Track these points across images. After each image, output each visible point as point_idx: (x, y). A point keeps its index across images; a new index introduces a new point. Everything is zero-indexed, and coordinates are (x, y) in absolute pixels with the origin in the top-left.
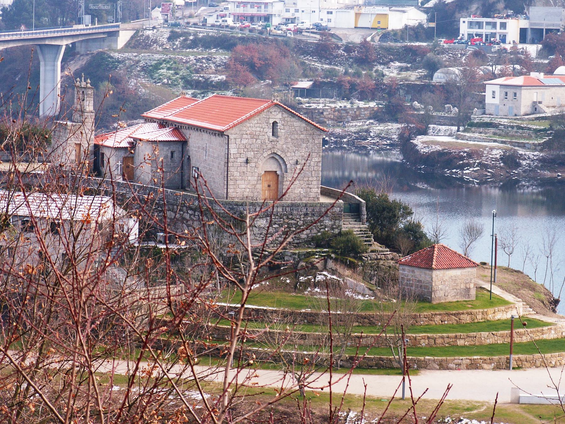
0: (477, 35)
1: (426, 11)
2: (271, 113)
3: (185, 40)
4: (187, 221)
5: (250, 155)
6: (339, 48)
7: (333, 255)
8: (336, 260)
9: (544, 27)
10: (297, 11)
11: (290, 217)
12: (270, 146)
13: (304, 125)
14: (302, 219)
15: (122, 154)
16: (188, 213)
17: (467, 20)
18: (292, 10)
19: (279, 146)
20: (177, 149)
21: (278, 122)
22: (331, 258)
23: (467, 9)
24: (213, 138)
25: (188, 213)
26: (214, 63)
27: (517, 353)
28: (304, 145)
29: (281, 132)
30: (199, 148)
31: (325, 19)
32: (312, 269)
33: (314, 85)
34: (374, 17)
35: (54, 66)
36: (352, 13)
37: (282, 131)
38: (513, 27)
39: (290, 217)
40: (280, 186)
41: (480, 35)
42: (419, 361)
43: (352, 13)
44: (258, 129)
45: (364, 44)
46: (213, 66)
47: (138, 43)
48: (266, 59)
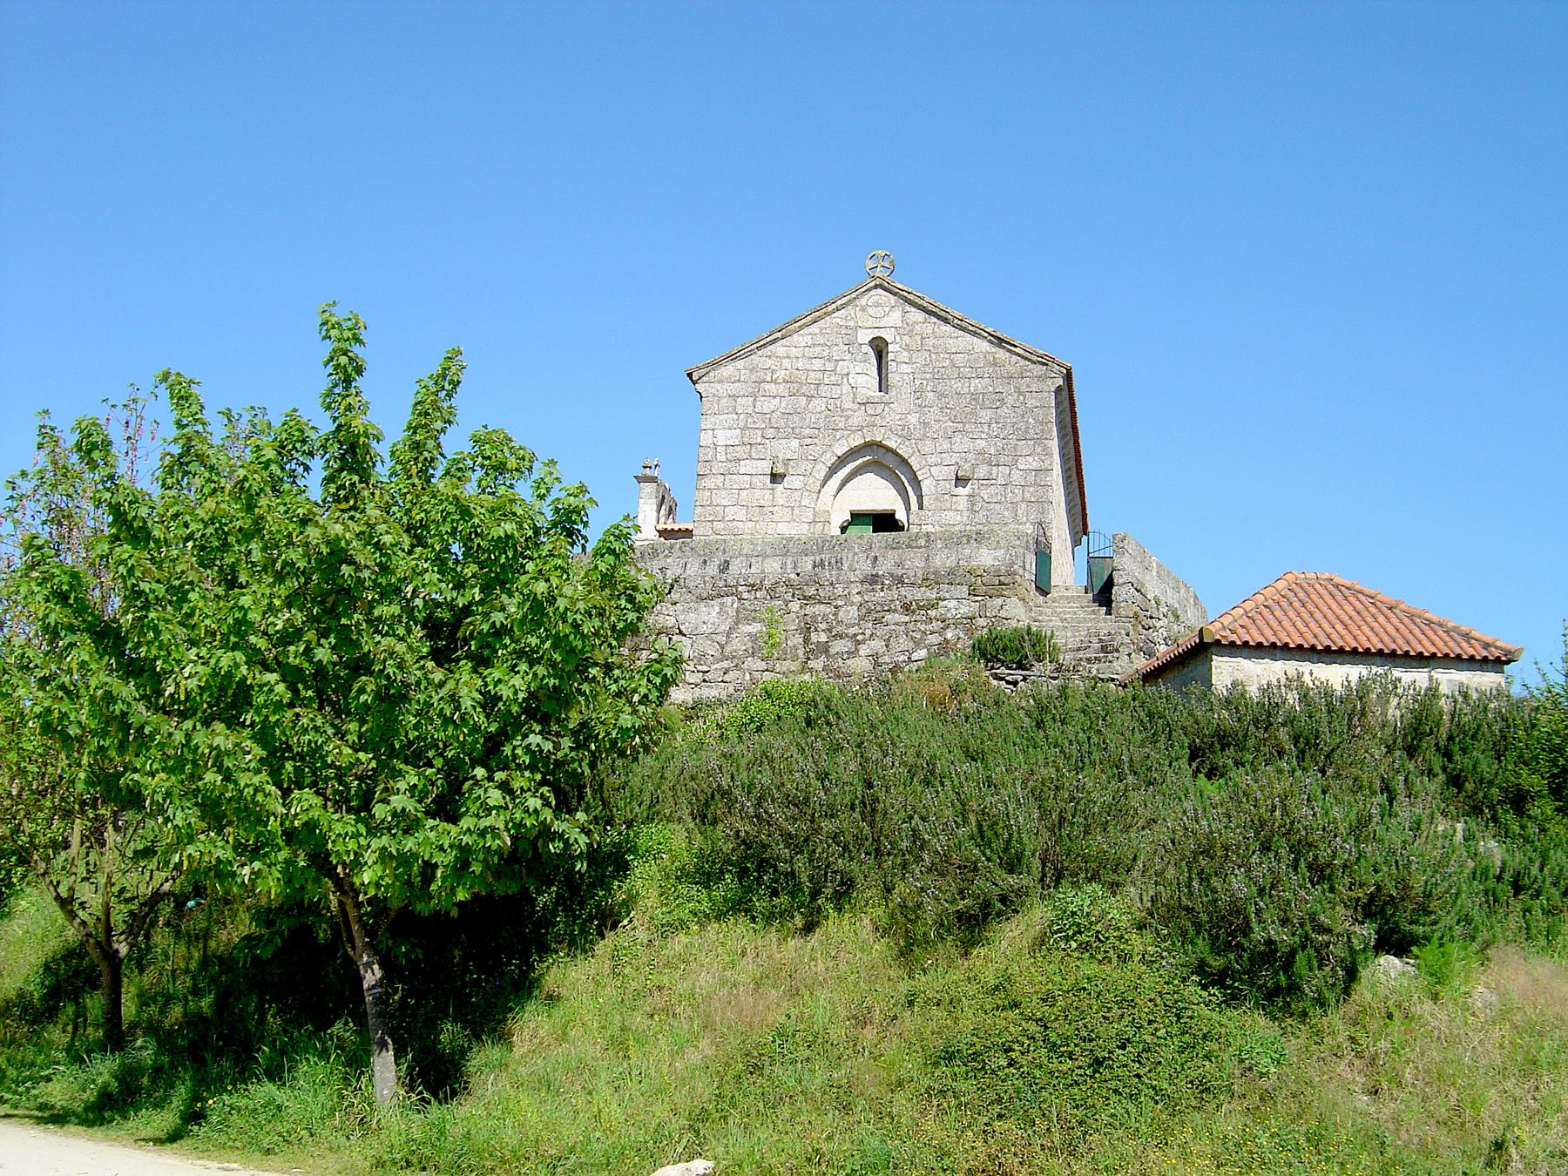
2: (863, 309)
12: (857, 418)
14: (857, 599)
21: (889, 339)
29: (899, 371)
37: (905, 368)
44: (817, 364)
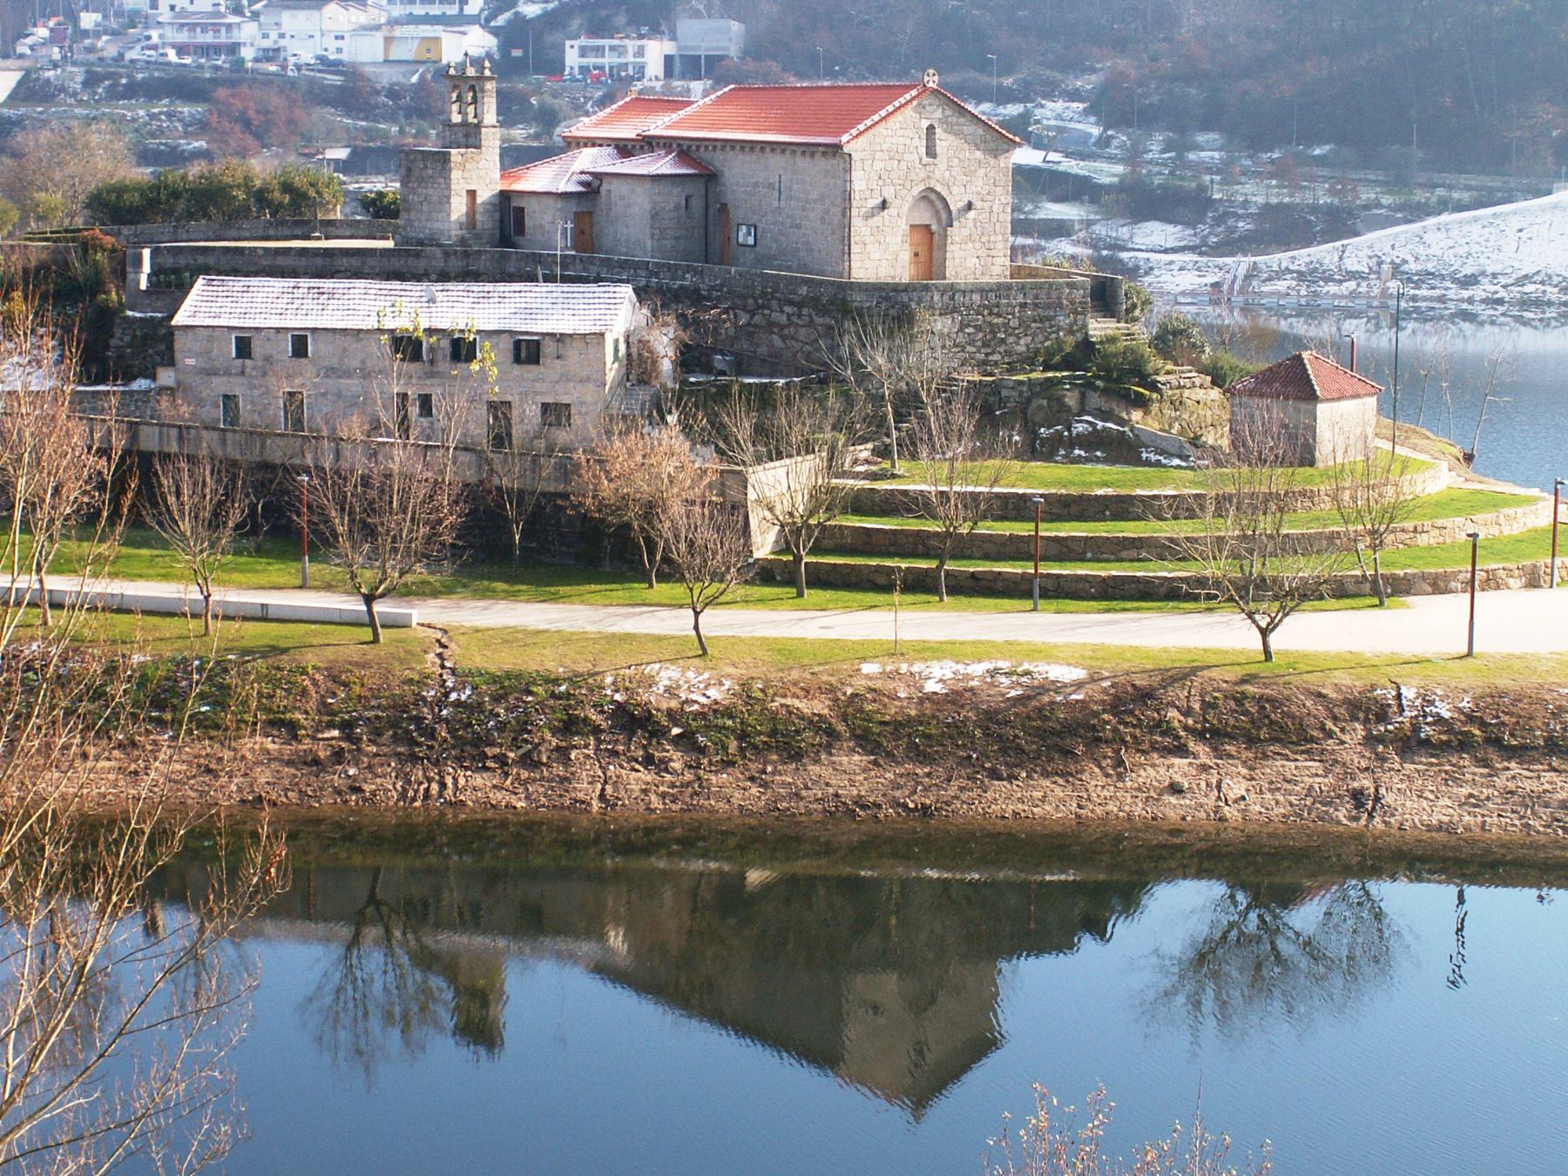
0: (595, 68)
1: (495, 32)
3: (115, 85)
4: (782, 327)
5: (888, 193)
6: (377, 93)
7: (1099, 383)
8: (1105, 392)
9: (703, 53)
10: (282, 36)
11: (995, 310)
13: (980, 131)
16: (782, 311)
17: (576, 43)
18: (274, 35)
19: (938, 174)
20: (697, 189)
22: (1096, 389)
23: (564, 27)
24: (803, 162)
25: (782, 311)
26: (179, 120)
28: (981, 172)
30: (756, 185)
31: (332, 48)
32: (1061, 414)
33: (354, 153)
34: (416, 43)
36: (379, 37)
38: (655, 52)
39: (995, 310)
40: (935, 254)
41: (601, 68)
43: (379, 37)
46: (179, 126)
48: (268, 112)
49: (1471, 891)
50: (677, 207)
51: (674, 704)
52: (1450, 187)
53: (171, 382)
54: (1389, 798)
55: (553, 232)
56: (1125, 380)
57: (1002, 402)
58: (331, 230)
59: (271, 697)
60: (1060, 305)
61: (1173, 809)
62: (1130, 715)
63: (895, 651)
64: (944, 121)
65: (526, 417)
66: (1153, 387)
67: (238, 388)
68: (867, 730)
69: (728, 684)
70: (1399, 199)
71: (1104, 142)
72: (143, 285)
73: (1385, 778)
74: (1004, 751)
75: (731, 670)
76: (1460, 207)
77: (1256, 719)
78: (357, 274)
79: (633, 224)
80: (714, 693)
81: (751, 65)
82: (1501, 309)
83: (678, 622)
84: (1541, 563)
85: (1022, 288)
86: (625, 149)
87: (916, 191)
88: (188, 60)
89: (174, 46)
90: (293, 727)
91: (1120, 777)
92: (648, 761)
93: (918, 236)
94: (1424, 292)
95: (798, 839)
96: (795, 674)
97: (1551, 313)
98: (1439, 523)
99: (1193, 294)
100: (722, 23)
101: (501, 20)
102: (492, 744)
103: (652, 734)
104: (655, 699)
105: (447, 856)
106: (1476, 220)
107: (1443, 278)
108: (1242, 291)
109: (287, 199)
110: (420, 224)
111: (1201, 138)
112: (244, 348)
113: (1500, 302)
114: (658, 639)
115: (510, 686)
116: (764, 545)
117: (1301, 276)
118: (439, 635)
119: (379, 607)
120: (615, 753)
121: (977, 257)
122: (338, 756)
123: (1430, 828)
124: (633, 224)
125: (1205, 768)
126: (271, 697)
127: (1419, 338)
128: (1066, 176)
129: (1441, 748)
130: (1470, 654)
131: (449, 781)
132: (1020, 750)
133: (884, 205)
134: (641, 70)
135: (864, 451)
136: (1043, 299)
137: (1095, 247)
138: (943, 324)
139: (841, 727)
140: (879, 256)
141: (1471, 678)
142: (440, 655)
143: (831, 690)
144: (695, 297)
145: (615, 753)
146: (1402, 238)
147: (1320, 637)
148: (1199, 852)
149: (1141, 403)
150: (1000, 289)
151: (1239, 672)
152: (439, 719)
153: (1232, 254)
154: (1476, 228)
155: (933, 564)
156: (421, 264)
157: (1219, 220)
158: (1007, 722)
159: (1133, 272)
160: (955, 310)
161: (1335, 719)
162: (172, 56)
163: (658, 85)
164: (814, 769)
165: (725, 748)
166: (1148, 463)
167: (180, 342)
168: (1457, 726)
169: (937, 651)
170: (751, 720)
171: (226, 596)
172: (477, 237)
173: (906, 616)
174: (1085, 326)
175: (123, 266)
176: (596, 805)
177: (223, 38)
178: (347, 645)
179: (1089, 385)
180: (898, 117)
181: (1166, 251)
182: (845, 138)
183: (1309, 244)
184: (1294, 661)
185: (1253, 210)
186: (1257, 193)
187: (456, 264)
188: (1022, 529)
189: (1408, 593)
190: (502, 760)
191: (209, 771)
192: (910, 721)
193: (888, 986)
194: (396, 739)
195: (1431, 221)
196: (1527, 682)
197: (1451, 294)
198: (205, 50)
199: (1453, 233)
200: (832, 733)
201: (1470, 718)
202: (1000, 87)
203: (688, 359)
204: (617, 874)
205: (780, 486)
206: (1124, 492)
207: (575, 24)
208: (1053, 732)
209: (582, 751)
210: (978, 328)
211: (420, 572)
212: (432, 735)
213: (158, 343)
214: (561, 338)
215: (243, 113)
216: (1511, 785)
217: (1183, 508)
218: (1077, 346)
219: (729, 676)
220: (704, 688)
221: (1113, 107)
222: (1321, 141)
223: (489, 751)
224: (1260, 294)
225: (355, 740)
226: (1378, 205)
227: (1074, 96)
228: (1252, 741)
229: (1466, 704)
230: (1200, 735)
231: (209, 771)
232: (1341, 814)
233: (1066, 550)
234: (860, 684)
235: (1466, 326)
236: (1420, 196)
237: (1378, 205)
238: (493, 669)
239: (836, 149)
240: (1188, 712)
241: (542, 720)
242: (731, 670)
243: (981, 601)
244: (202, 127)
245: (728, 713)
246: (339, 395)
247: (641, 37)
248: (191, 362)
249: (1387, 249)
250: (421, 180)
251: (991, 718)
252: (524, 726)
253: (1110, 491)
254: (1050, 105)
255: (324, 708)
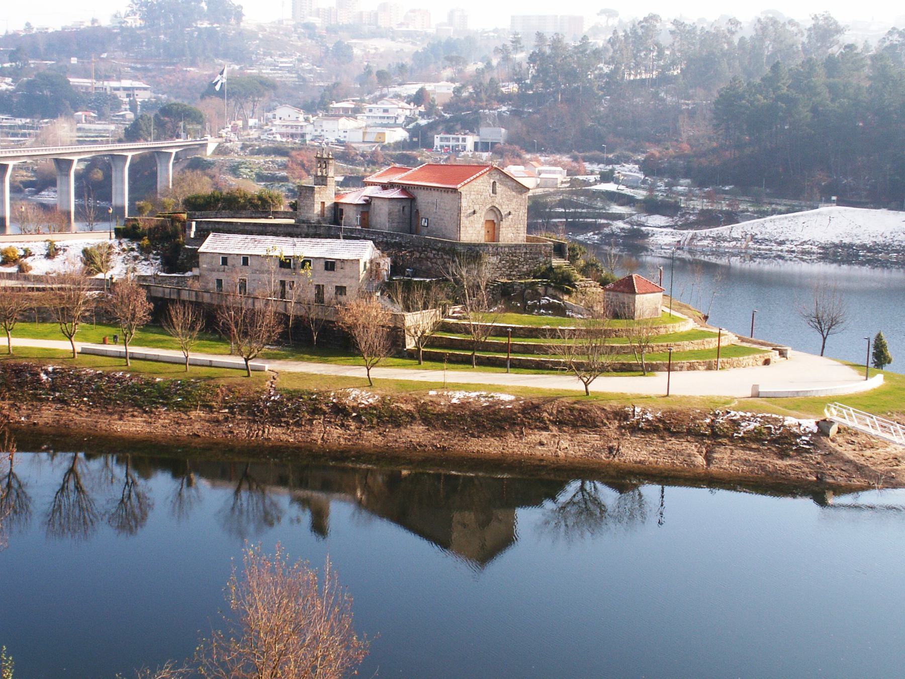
1: (408, 131)
5: (477, 208)
8: (554, 288)
9: (490, 141)
15: (360, 209)
18: (319, 130)
22: (551, 286)
24: (445, 195)
27: (723, 357)
32: (537, 296)
35: (168, 166)
38: (471, 140)
42: (652, 364)
43: (361, 132)
45: (373, 153)
47: (221, 150)
49: (666, 488)
50: (399, 211)
51: (355, 404)
52: (777, 204)
53: (197, 274)
54: (622, 450)
55: (352, 218)
56: (563, 283)
57: (514, 291)
58: (277, 215)
59: (204, 396)
60: (541, 253)
61: (539, 451)
62: (531, 414)
63: (444, 386)
64: (500, 180)
65: (329, 292)
66: (574, 286)
67: (222, 276)
68: (427, 417)
69: (377, 397)
70: (756, 209)
71: (644, 182)
72: (192, 236)
73: (623, 442)
74: (478, 427)
75: (379, 392)
76: (780, 213)
77: (577, 417)
78: (276, 234)
79: (382, 219)
80: (371, 400)
81: (508, 147)
82: (794, 255)
83: (360, 372)
84: (713, 360)
85: (530, 246)
86: (385, 187)
87: (488, 207)
88: (284, 140)
89: (280, 134)
90: (211, 407)
91: (521, 438)
92: (342, 425)
93: (489, 225)
94: (763, 247)
95: (398, 457)
96: (403, 394)
97: (814, 257)
98: (678, 343)
99: (669, 245)
100: (497, 129)
101: (411, 126)
102: (285, 417)
103: (345, 415)
104: (348, 402)
105: (269, 459)
106: (786, 218)
107: (771, 241)
108: (689, 244)
109: (260, 203)
110: (304, 214)
111: (682, 181)
112: (225, 261)
113: (793, 252)
114: (357, 379)
115: (293, 395)
116: (410, 344)
117: (714, 239)
118: (274, 374)
119: (250, 363)
120: (330, 422)
121: (514, 233)
122: (226, 419)
123: (636, 462)
124: (382, 219)
125: (555, 436)
126: (204, 396)
127: (762, 265)
128: (624, 196)
129: (646, 431)
130: (668, 395)
131: (266, 430)
132: (484, 426)
133: (474, 212)
134: (464, 148)
135: (458, 308)
136: (534, 250)
137: (632, 225)
138: (494, 260)
139: (417, 415)
140: (472, 232)
141: (664, 405)
142: (272, 383)
143: (416, 400)
144: (399, 246)
145: (330, 422)
146: (756, 225)
147: (607, 386)
148: (553, 469)
149: (568, 293)
150: (517, 246)
151: (574, 399)
152: (266, 407)
153: (687, 229)
154: (786, 221)
155: (470, 353)
156: (299, 230)
157: (682, 215)
158: (480, 416)
159: (646, 235)
160: (498, 254)
161: (608, 419)
162: (279, 138)
163: (470, 154)
164: (404, 431)
165: (372, 421)
166: (568, 316)
167: (202, 259)
168: (654, 423)
169: (458, 387)
170: (383, 411)
171: (194, 356)
172: (324, 220)
173: (448, 373)
174: (551, 262)
175: (186, 226)
176: (320, 442)
177: (299, 131)
178: (238, 377)
179: (548, 285)
180: (481, 178)
181: (661, 227)
182: (459, 186)
183: (718, 226)
184: (598, 396)
185: (696, 212)
186: (699, 205)
187: (312, 231)
188: (503, 340)
189: (657, 370)
190: (287, 423)
191: (177, 423)
192: (444, 414)
193: (470, 517)
194: (249, 414)
195: (768, 218)
196: (683, 408)
197: (774, 248)
198: (293, 136)
199: (777, 223)
200: (413, 417)
201: (659, 420)
202: (607, 158)
203: (395, 269)
204: (333, 467)
205: (419, 322)
206: (553, 327)
207: (440, 128)
208: (498, 420)
209: (318, 421)
210: (507, 262)
211: (275, 350)
212: (262, 412)
213: (194, 258)
214: (343, 261)
215: (302, 161)
216: (670, 447)
217: (553, 333)
218: (547, 269)
219: (378, 394)
220: (367, 398)
221: (650, 168)
222: (728, 184)
223: (283, 419)
224: (697, 246)
225: (233, 413)
226: (748, 211)
227: (636, 162)
228: (574, 426)
229: (659, 415)
230: (554, 423)
231: (177, 423)
232: (603, 456)
233: (527, 350)
234: (427, 399)
235: (780, 261)
236: (766, 208)
237: (748, 211)
238: (289, 388)
239: (455, 190)
240: (551, 414)
241: (304, 408)
242: (379, 392)
243: (489, 368)
244: (285, 167)
245: (375, 408)
246: (259, 280)
247: (465, 134)
248: (205, 266)
249: (749, 229)
250: (305, 197)
251: (475, 414)
252: (297, 409)
253: (548, 327)
254: (627, 166)
255: (224, 401)
